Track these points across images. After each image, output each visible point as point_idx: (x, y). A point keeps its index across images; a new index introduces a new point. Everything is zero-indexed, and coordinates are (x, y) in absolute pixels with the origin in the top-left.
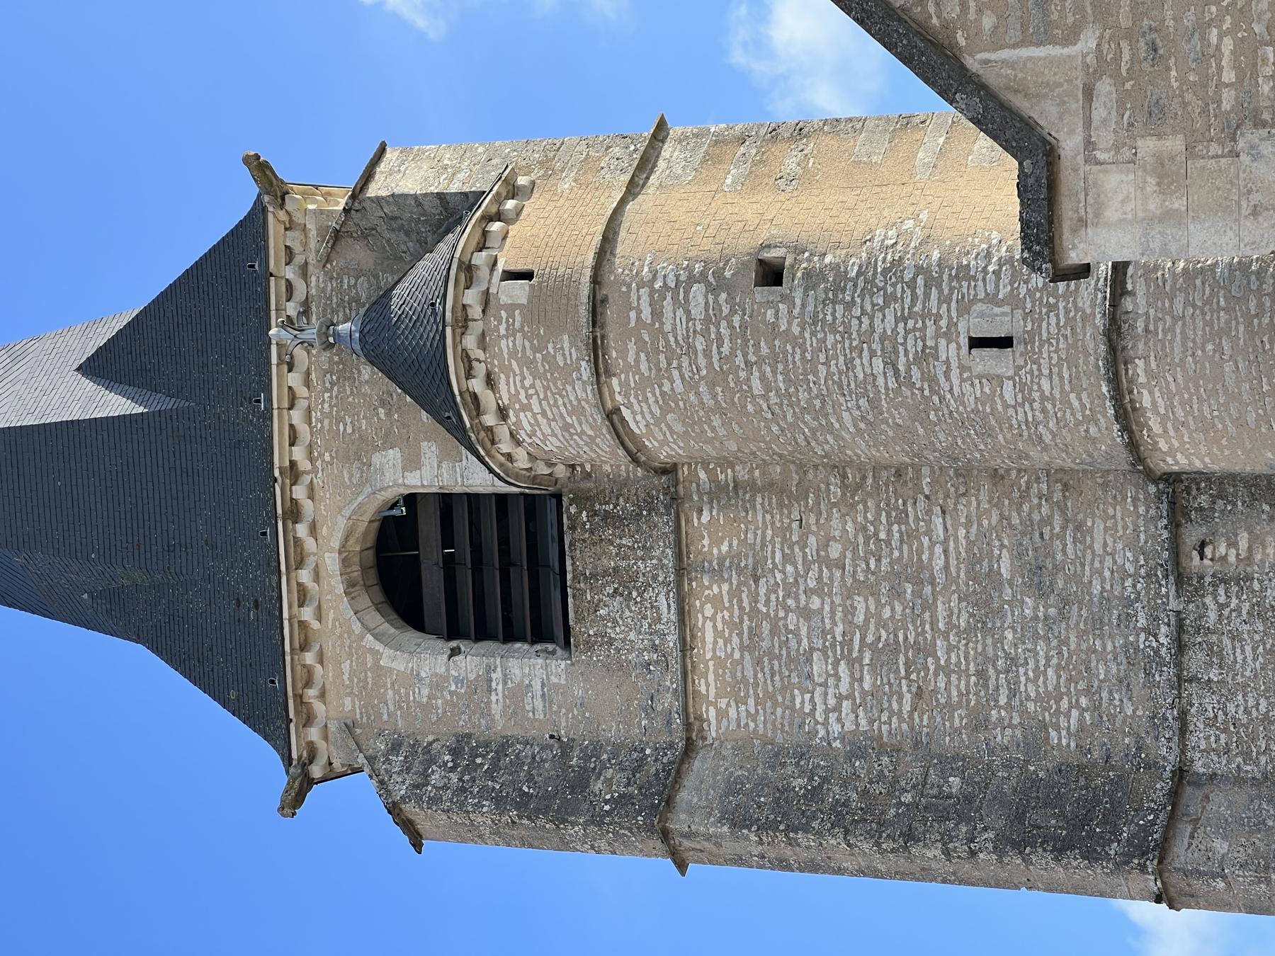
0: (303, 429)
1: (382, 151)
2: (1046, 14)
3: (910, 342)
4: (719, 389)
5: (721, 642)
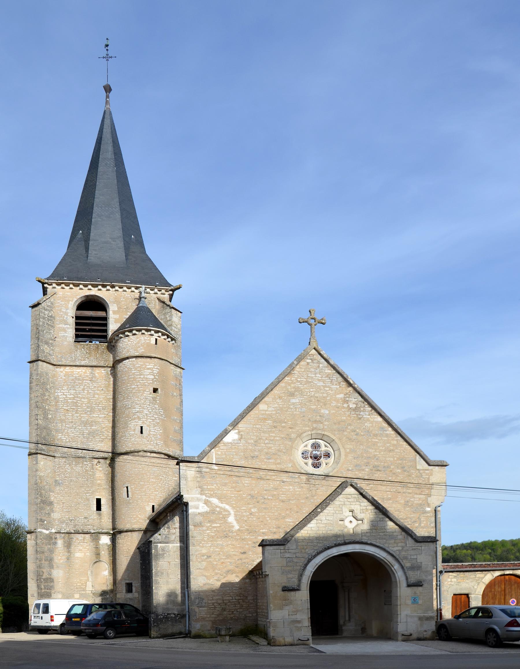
3: (142, 416)
4: (132, 379)
5: (77, 373)
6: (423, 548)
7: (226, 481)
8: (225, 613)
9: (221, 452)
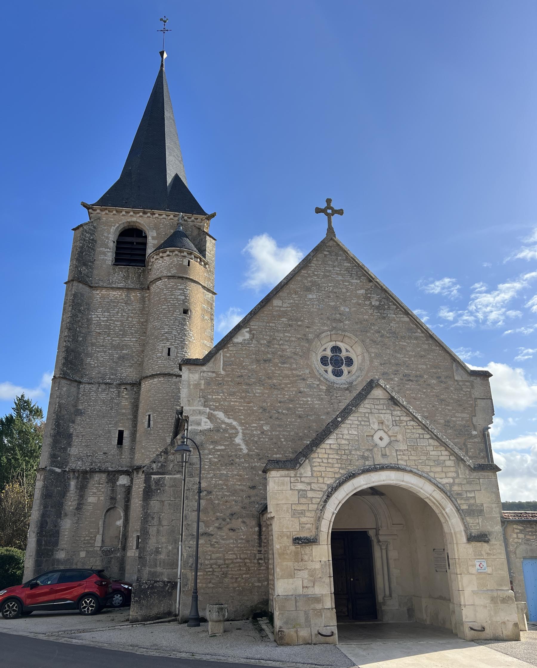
0: (162, 217)
2: (228, 365)
6: (481, 480)
7: (234, 390)
8: (226, 580)
9: (230, 353)
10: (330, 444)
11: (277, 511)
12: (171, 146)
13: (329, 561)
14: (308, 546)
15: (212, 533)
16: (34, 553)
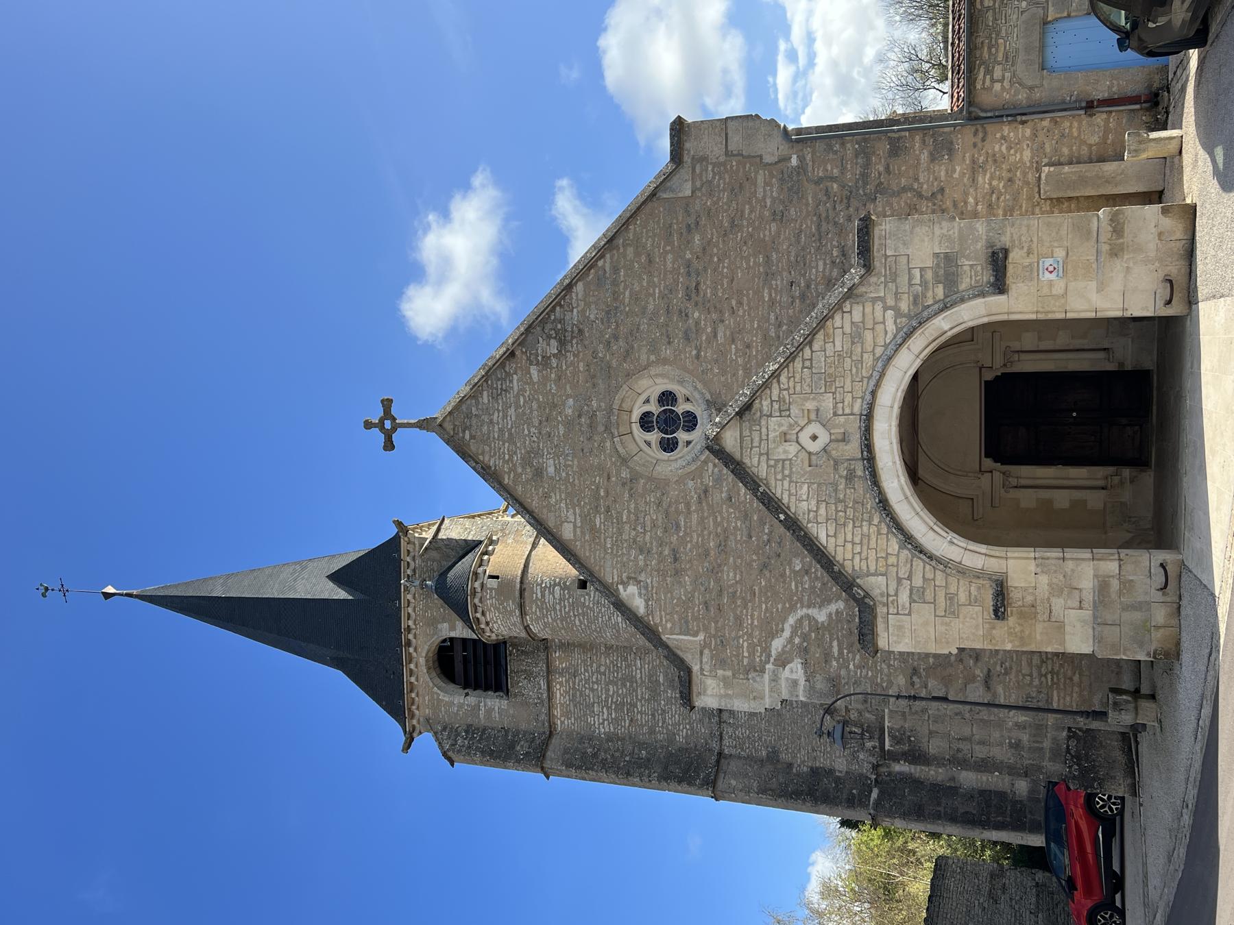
0: (413, 614)
1: (443, 519)
2: (688, 626)
6: (889, 253)
9: (666, 621)
10: (828, 536)
11: (948, 643)
12: (277, 586)
13: (1035, 558)
14: (1008, 594)
15: (985, 671)
16: (1019, 834)
